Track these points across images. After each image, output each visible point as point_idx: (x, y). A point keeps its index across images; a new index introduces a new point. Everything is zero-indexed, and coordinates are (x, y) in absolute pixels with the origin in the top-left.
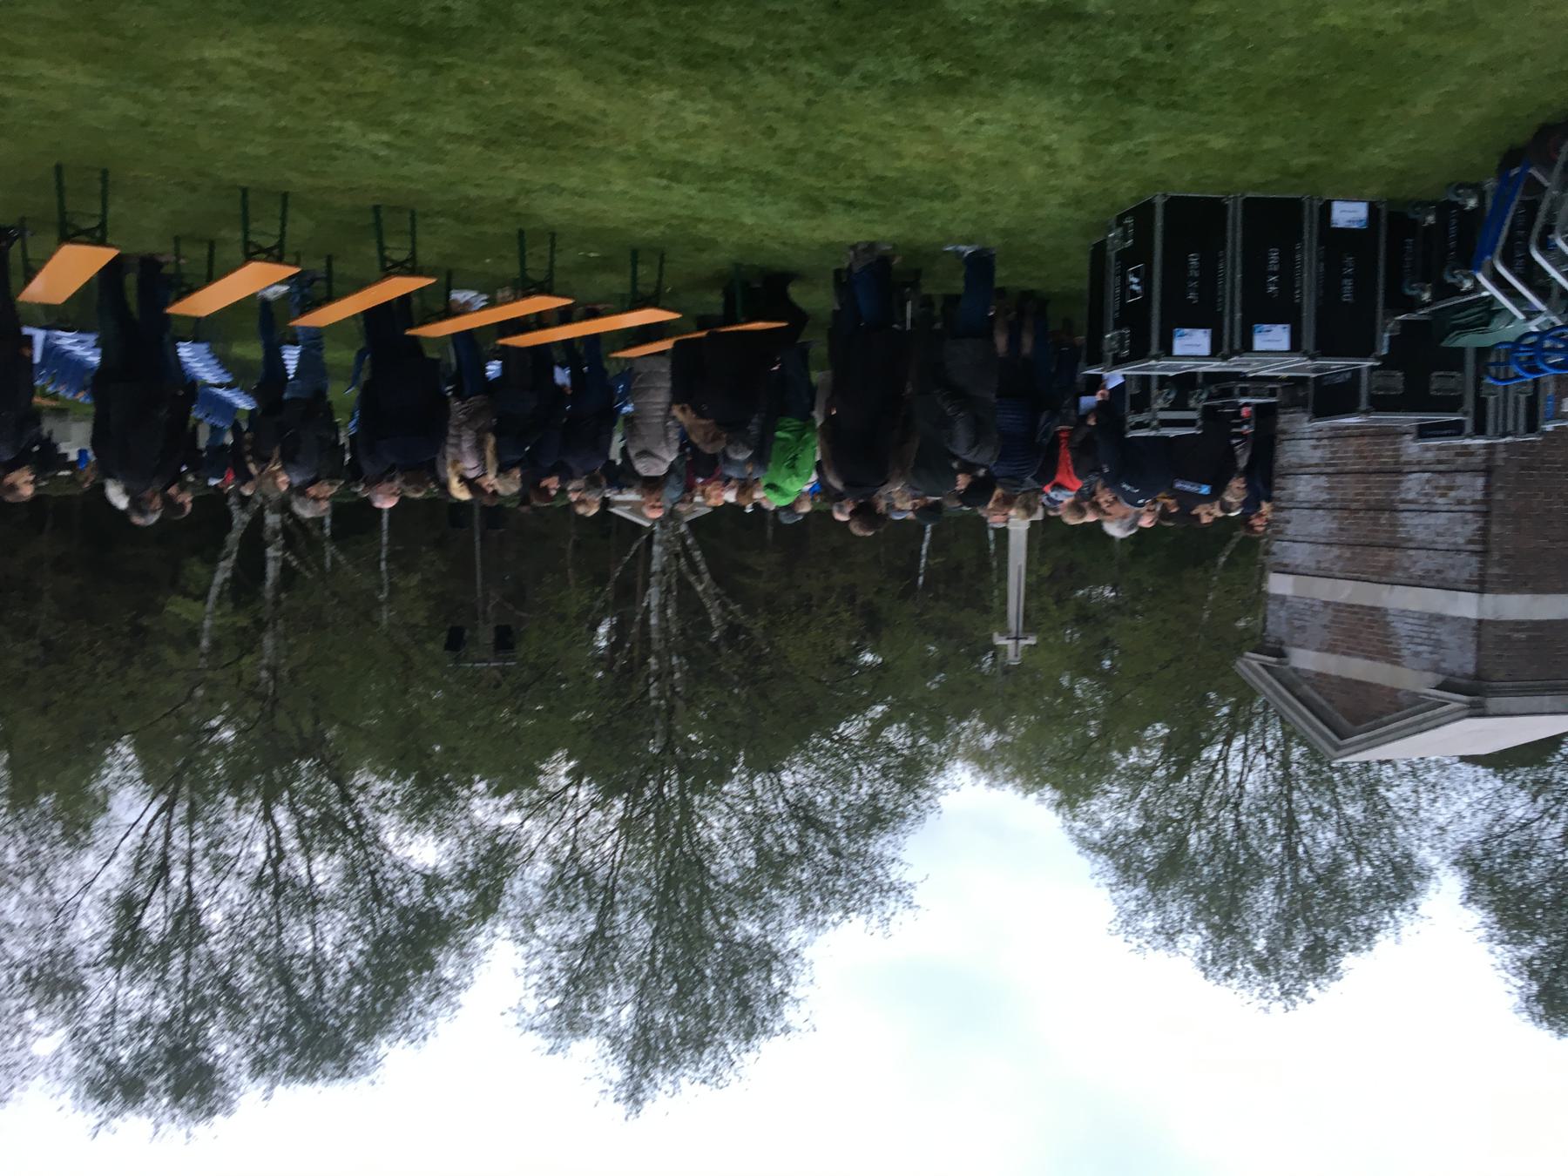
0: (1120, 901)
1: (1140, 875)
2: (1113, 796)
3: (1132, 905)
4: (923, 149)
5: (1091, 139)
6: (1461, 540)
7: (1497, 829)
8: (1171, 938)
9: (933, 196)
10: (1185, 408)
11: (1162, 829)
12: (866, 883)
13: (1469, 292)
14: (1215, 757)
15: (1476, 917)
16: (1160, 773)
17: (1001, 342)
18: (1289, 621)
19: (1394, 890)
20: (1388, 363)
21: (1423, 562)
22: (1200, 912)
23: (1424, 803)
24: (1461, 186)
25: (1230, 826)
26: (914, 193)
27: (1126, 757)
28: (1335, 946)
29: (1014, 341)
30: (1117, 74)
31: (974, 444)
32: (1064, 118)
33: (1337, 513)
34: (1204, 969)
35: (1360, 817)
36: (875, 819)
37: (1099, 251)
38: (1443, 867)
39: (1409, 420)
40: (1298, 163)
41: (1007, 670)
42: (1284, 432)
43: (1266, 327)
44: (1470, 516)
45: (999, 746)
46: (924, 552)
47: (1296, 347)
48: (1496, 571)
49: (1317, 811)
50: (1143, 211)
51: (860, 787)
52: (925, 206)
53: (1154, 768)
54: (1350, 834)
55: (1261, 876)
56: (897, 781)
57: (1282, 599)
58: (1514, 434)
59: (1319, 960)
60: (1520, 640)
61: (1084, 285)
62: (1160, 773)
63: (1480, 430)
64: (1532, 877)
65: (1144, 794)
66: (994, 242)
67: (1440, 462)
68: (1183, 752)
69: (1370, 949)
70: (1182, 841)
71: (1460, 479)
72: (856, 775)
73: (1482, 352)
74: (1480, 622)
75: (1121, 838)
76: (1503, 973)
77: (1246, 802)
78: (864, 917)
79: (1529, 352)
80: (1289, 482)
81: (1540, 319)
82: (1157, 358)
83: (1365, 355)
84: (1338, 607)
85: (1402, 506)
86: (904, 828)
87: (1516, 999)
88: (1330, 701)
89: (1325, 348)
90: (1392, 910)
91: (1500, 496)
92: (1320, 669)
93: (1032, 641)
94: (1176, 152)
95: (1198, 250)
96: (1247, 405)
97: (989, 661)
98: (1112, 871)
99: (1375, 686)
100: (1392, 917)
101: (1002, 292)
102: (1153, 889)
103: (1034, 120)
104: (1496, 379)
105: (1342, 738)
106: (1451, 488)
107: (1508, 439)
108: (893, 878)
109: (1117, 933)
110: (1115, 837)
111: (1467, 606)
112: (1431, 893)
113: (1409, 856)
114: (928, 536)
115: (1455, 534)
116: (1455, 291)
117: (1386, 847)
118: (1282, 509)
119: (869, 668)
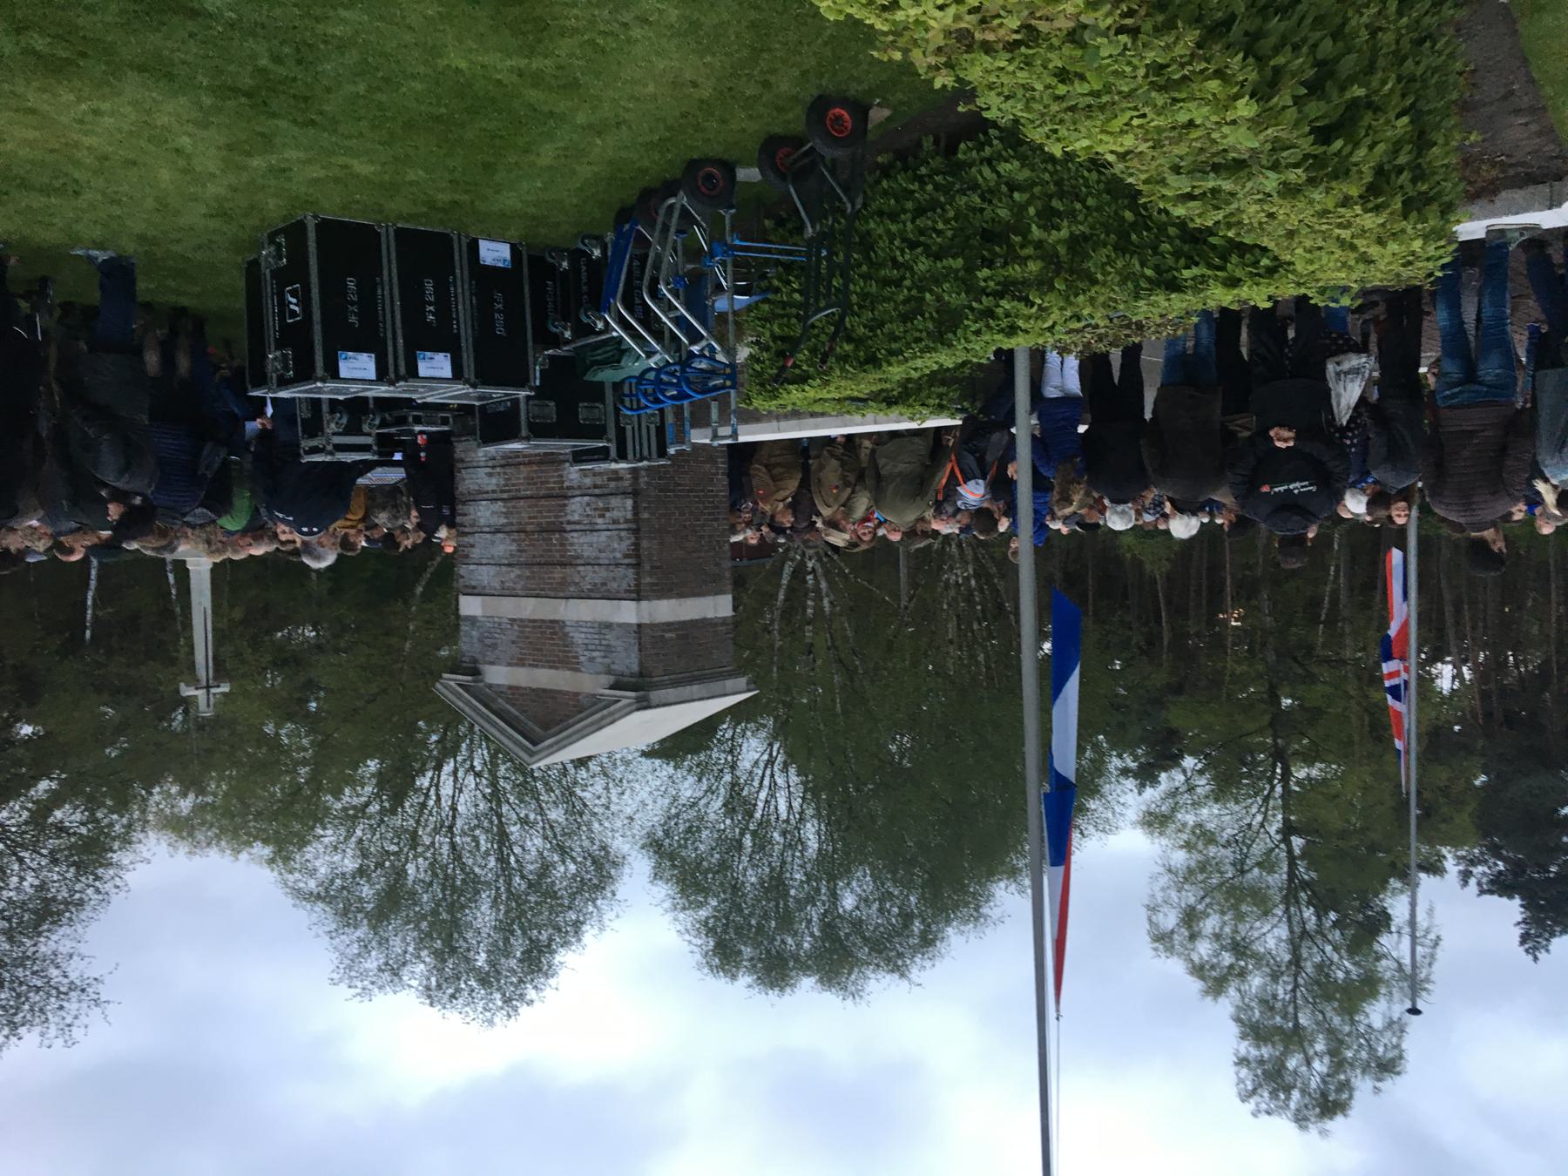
0: (342, 948)
1: (360, 916)
2: (326, 840)
3: (355, 949)
4: (31, 134)
5: (230, 147)
6: (618, 555)
7: (673, 811)
8: (395, 973)
9: (46, 191)
10: (360, 433)
11: (380, 865)
12: (38, 989)
13: (601, 332)
14: (426, 784)
15: (663, 890)
16: (374, 808)
17: (152, 360)
18: (481, 640)
19: (595, 881)
20: (541, 394)
21: (591, 576)
22: (423, 940)
23: (614, 799)
24: (589, 237)
25: (445, 849)
26: (25, 185)
27: (339, 800)
28: (549, 946)
29: (168, 360)
30: (247, 82)
31: (126, 469)
32: (196, 123)
33: (515, 536)
34: (429, 997)
35: (562, 819)
36: (47, 912)
37: (253, 268)
38: (634, 853)
39: (566, 446)
40: (443, 198)
41: (202, 725)
42: (462, 461)
43: (429, 354)
44: (623, 534)
45: (199, 809)
46: (89, 602)
47: (458, 374)
48: (648, 580)
49: (524, 821)
50: (295, 231)
51: (22, 879)
52: (37, 201)
53: (367, 804)
54: (555, 836)
55: (477, 892)
56: (74, 864)
57: (472, 620)
58: (649, 460)
59: (536, 962)
60: (671, 639)
61: (240, 304)
62: (374, 808)
63: (622, 456)
64: (702, 847)
65: (359, 833)
66: (130, 247)
67: (596, 486)
68: (396, 785)
69: (579, 940)
70: (401, 873)
71: (615, 502)
72: (16, 867)
73: (617, 386)
74: (639, 625)
75: (338, 881)
76: (687, 937)
77: (459, 823)
78: (37, 1030)
79: (651, 385)
80: (470, 509)
81: (657, 358)
82: (323, 380)
83: (522, 383)
84: (522, 623)
85: (569, 528)
86: (83, 916)
87: (698, 957)
88: (523, 712)
89: (485, 376)
90: (594, 901)
91: (646, 516)
92: (514, 683)
93: (225, 688)
94: (331, 171)
95: (356, 274)
96: (421, 432)
97: (180, 718)
98: (331, 918)
99: (559, 692)
100: (595, 906)
101: (148, 307)
102: (374, 928)
103: (163, 120)
104: (631, 409)
105: (535, 744)
106: (607, 510)
107: (645, 463)
108: (73, 976)
109: (341, 980)
110: (332, 882)
111: (628, 613)
112: (626, 878)
113: (604, 848)
114: (93, 584)
115: (614, 550)
116: (591, 331)
117: (586, 843)
118: (465, 534)
119: (28, 741)
